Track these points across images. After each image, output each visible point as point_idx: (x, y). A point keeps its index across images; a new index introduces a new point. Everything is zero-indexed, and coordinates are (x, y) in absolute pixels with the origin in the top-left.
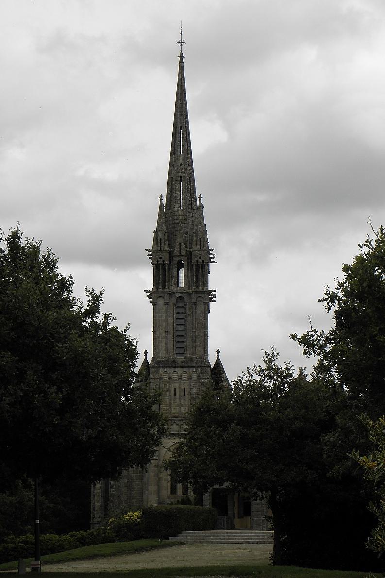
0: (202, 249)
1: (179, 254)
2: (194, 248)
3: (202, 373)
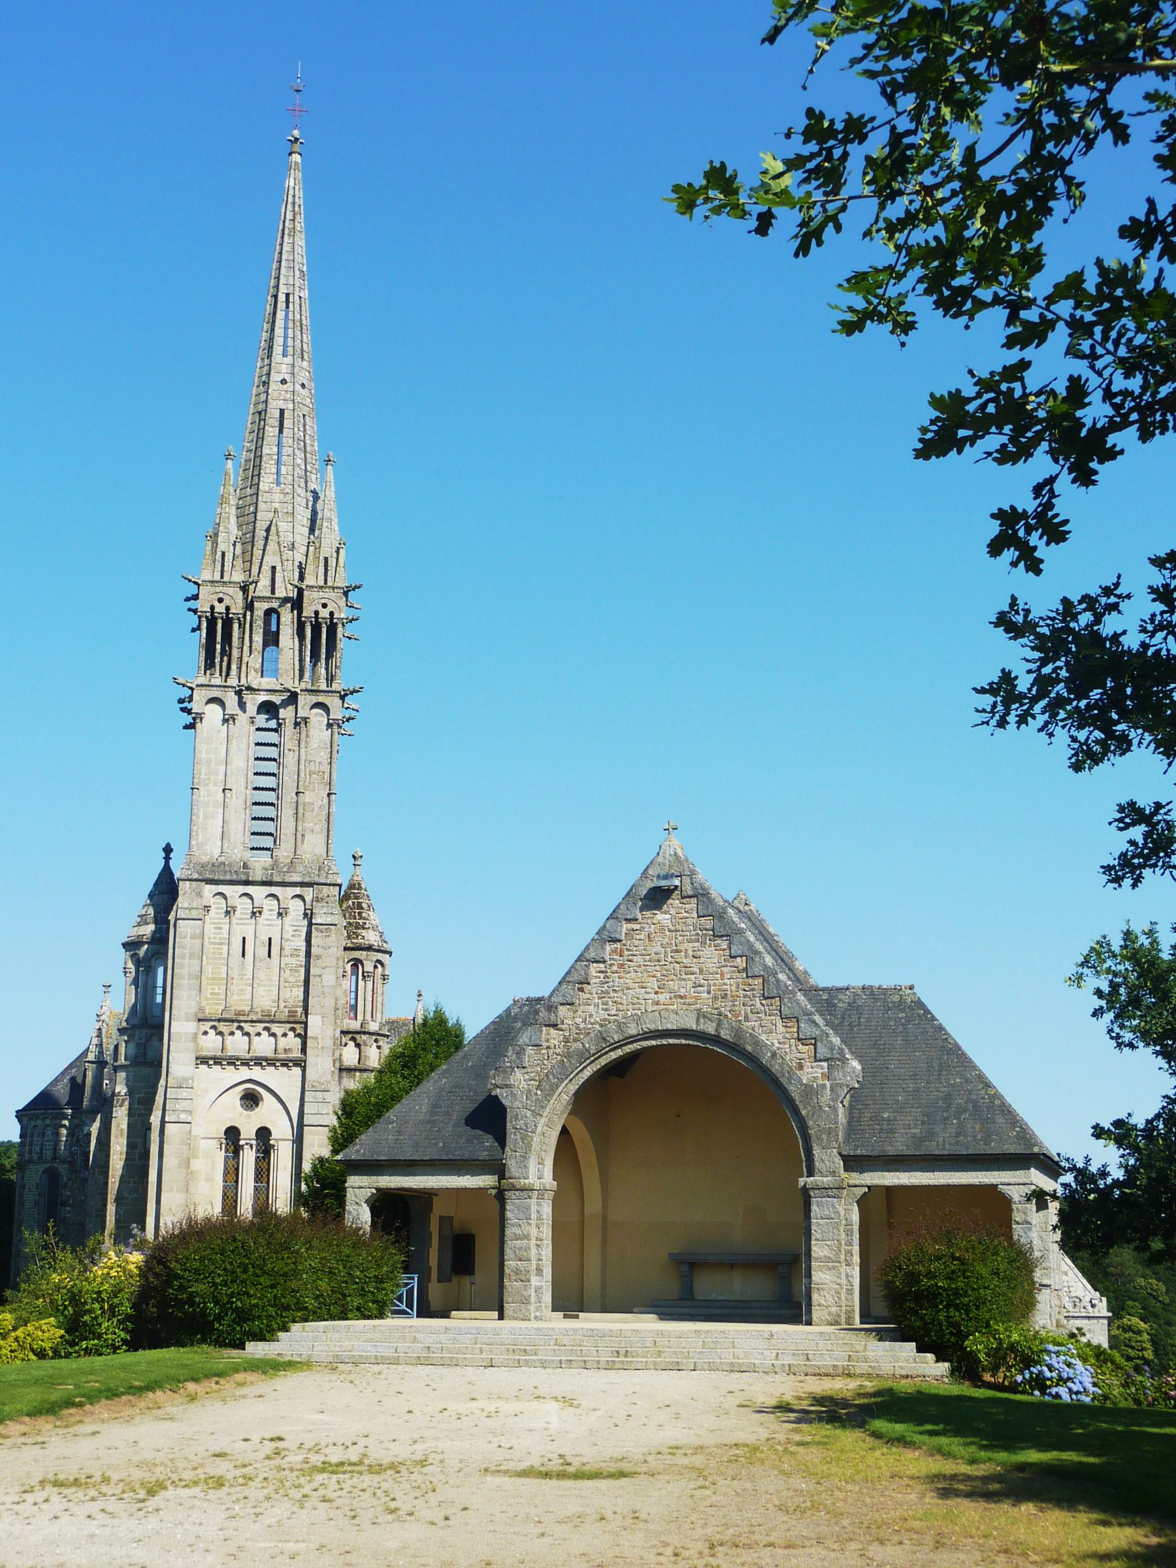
0: (330, 584)
1: (269, 594)
2: (309, 580)
3: (317, 900)
